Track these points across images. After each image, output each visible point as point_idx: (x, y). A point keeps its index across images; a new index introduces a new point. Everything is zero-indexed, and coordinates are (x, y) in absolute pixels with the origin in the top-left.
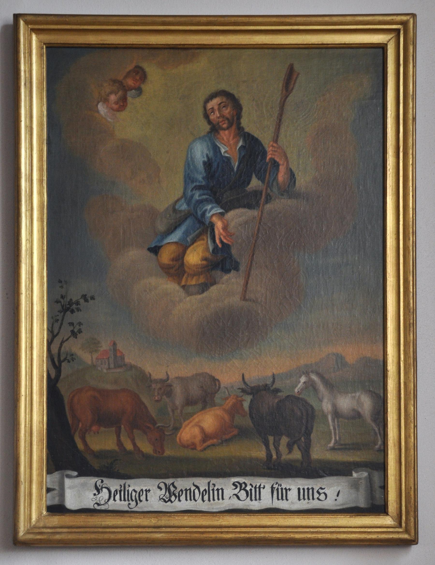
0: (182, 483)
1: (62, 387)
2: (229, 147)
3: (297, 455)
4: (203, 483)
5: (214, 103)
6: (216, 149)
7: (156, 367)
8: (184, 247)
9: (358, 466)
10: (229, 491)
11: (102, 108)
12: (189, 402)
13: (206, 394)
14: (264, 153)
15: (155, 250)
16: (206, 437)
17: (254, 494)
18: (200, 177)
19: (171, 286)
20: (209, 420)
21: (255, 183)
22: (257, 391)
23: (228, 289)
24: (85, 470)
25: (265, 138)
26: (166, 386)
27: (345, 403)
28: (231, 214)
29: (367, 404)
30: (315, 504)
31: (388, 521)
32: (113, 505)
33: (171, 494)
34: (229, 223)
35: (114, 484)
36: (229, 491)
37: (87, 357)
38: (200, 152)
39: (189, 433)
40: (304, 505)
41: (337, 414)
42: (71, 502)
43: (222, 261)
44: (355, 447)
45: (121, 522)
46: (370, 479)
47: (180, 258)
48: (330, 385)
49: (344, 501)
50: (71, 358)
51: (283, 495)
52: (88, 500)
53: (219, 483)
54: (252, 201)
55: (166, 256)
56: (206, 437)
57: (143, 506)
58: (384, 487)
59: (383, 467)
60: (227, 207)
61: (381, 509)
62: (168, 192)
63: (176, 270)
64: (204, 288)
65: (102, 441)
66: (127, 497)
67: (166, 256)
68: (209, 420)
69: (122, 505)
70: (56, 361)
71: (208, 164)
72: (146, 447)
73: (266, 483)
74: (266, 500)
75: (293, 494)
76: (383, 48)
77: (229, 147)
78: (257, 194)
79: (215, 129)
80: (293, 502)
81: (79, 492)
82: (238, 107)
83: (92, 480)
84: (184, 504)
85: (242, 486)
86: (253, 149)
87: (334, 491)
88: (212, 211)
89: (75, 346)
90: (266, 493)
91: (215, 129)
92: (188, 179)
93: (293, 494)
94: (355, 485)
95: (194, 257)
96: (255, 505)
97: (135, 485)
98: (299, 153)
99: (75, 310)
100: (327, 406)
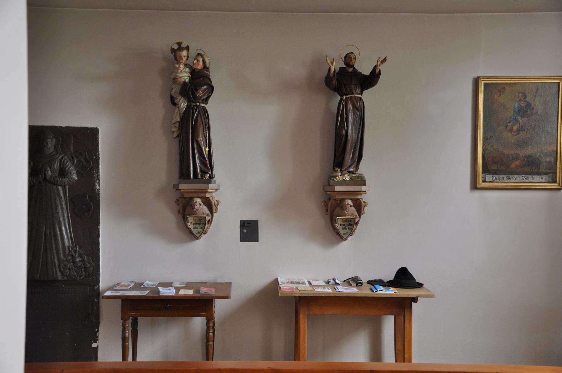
0: (511, 176)
1: (486, 156)
2: (523, 104)
3: (537, 170)
4: (516, 176)
5: (520, 95)
6: (520, 105)
7: (506, 152)
8: (513, 126)
9: (550, 173)
10: (521, 178)
11: (496, 96)
12: (513, 159)
13: (516, 158)
14: (531, 105)
15: (506, 126)
16: (517, 166)
17: (527, 179)
18: (517, 110)
19: (510, 134)
20: (517, 163)
21: (529, 112)
22: (528, 157)
23: (522, 135)
24: (490, 173)
25: (531, 102)
26: (508, 156)
27: (548, 160)
28: (523, 119)
29: (552, 160)
30: (540, 181)
31: (557, 184)
32: (496, 181)
33: (509, 178)
34: (521, 120)
35: (497, 176)
36: (521, 178)
37: (491, 149)
38: (517, 105)
39: (513, 166)
40: (538, 181)
41: (546, 162)
42: (487, 180)
43: (521, 129)
44: (550, 169)
45: (330, 291)
46: (553, 176)
47: (512, 128)
48: (544, 156)
49: (546, 181)
50: (488, 150)
51: (533, 179)
52: (491, 180)
53: (519, 176)
54: (528, 116)
55: (509, 128)
56: (517, 166)
57: (503, 181)
58: (556, 177)
59: (556, 173)
60: (523, 117)
61: (556, 182)
62: (510, 114)
63: (511, 131)
64: (517, 135)
65: (494, 167)
66: (499, 179)
67: (509, 128)
68: (517, 163)
69: (498, 181)
70: (484, 150)
71: (518, 108)
72: (503, 168)
73: (530, 176)
74: (530, 180)
75: (536, 179)
76: (559, 83)
77: (523, 104)
78: (529, 114)
79: (520, 100)
80: (535, 180)
81: (489, 178)
82: (525, 96)
83: (492, 175)
84: (512, 181)
85: (524, 177)
86: (529, 106)
87: (544, 178)
88: (519, 118)
89: (488, 147)
90: (530, 178)
91: (520, 100)
92: (514, 111)
93: (536, 179)
94: (549, 177)
95: (515, 128)
96: (527, 181)
97: (501, 176)
98: (538, 106)
99: (189, 104)
100: (543, 160)
